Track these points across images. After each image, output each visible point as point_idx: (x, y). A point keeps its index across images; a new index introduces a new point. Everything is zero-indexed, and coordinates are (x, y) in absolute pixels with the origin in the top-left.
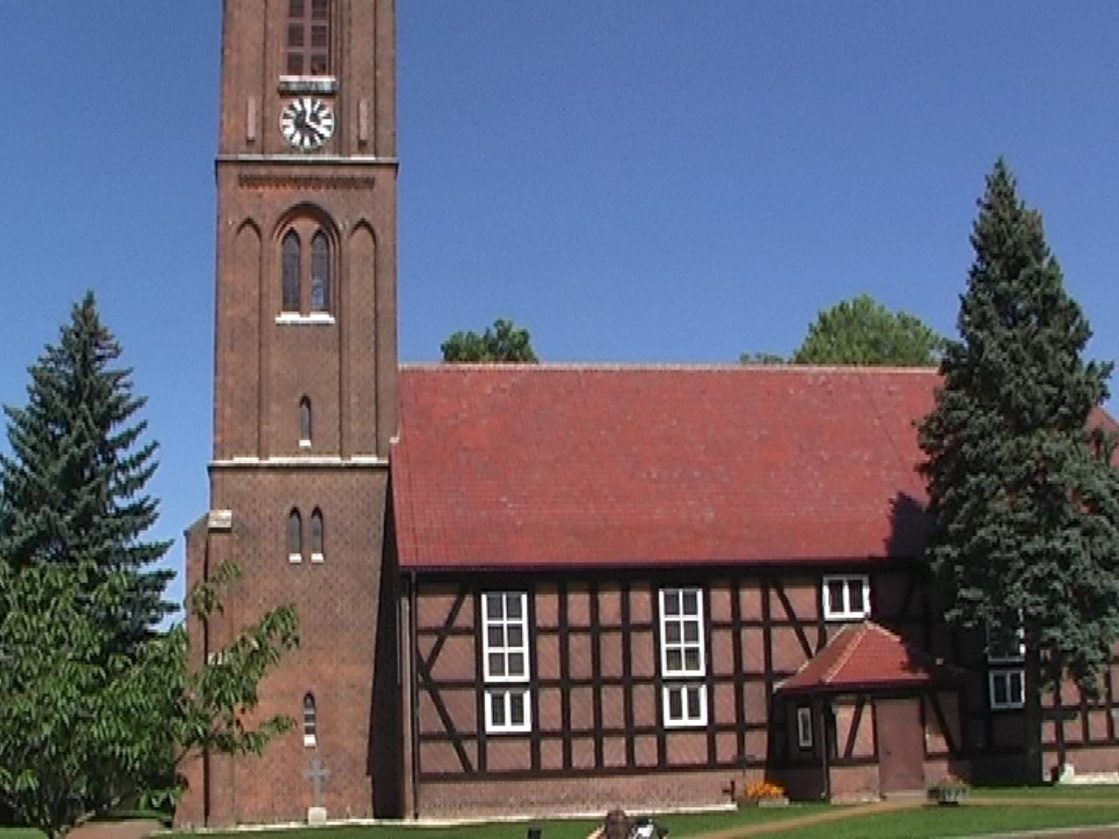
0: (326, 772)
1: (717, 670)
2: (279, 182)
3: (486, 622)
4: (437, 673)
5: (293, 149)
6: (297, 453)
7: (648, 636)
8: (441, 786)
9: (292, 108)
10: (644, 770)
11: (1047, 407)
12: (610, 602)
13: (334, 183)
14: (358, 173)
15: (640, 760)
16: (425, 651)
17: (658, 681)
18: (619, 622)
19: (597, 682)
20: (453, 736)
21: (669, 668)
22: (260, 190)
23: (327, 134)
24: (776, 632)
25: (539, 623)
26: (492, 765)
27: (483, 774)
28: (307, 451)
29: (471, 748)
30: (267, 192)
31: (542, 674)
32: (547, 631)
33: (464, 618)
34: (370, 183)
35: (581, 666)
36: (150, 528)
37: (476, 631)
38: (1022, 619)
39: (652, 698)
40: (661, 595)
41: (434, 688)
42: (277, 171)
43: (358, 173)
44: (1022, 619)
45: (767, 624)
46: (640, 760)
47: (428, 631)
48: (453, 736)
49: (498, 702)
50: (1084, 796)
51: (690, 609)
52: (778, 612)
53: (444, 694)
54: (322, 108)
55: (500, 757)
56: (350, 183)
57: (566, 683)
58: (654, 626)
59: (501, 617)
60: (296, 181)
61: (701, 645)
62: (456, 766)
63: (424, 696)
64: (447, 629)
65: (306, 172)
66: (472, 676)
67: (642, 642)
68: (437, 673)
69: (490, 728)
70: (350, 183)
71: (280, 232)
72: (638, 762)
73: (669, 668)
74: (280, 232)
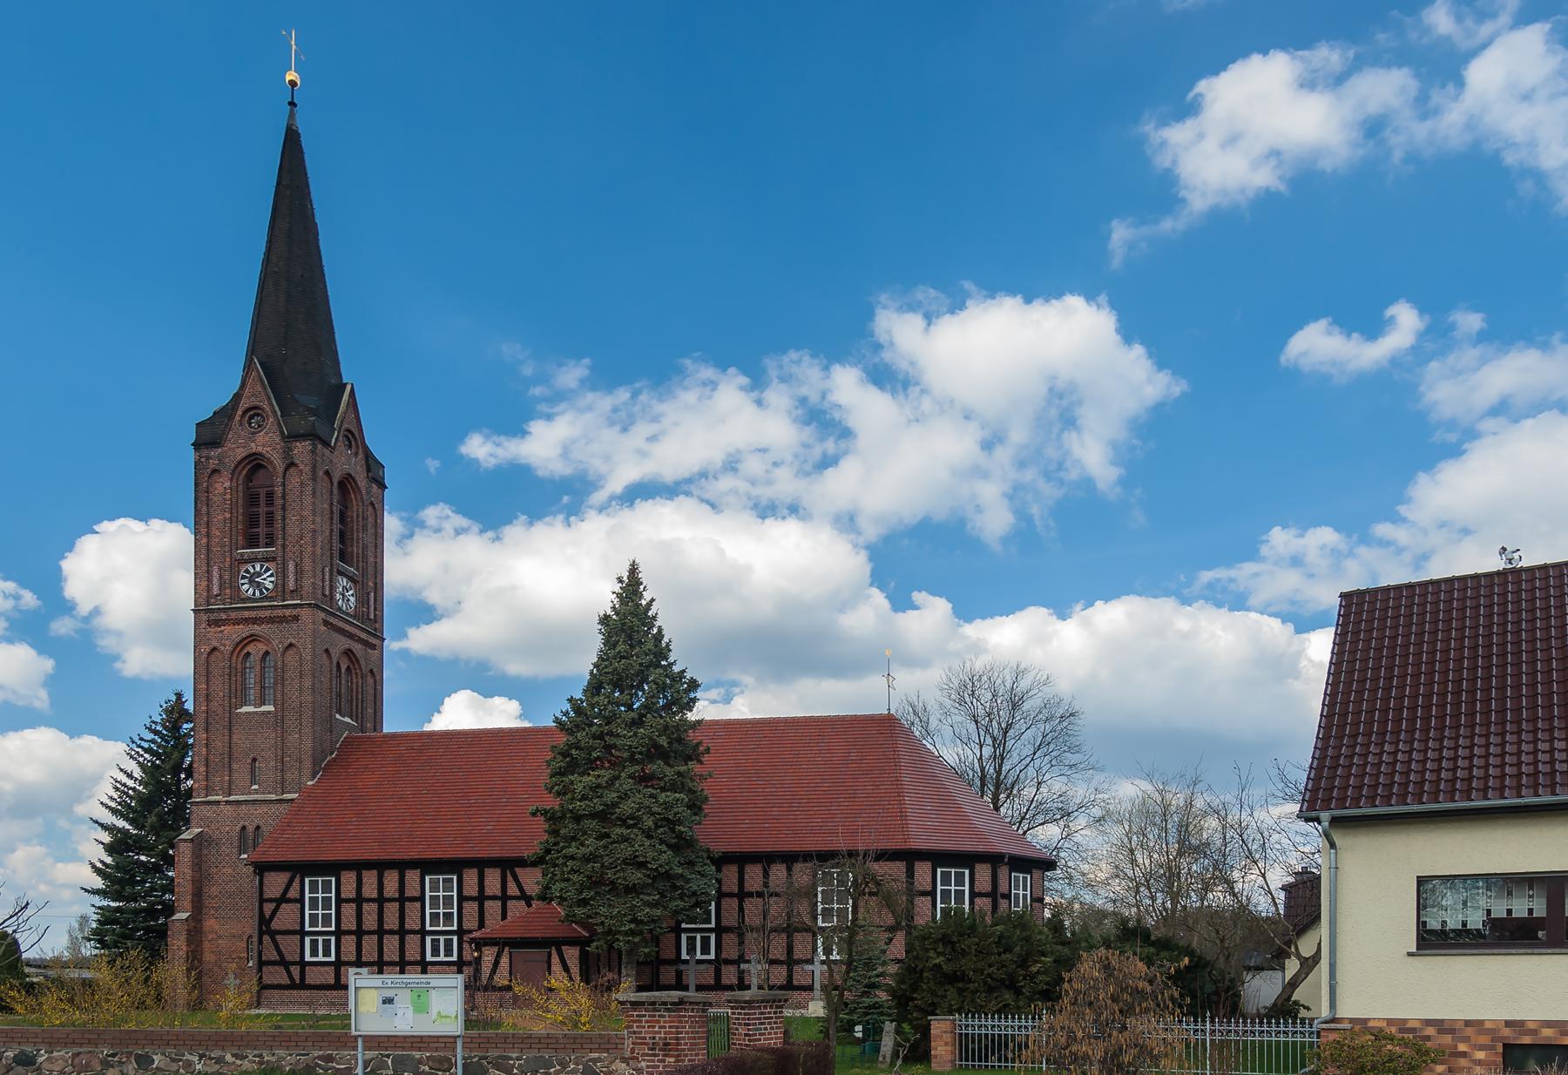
1: (344, 927)
2: (237, 622)
4: (275, 925)
5: (249, 599)
7: (418, 905)
8: (275, 992)
9: (247, 571)
10: (730, 988)
12: (391, 880)
13: (271, 620)
14: (288, 612)
15: (725, 981)
16: (267, 913)
17: (423, 933)
18: (397, 895)
19: (381, 932)
20: (283, 962)
21: (710, 923)
22: (223, 628)
23: (270, 586)
24: (510, 904)
25: (343, 896)
26: (308, 981)
27: (303, 986)
29: (295, 970)
30: (227, 629)
31: (725, 923)
32: (348, 901)
33: (293, 893)
34: (296, 618)
35: (370, 922)
37: (301, 901)
39: (419, 943)
40: (307, 880)
41: (273, 934)
42: (233, 615)
43: (288, 612)
45: (504, 898)
46: (725, 981)
47: (270, 900)
48: (283, 962)
52: (513, 889)
53: (278, 937)
54: (268, 570)
55: (313, 976)
58: (422, 899)
60: (246, 621)
62: (286, 981)
63: (266, 938)
64: (283, 899)
66: (298, 928)
67: (412, 909)
68: (275, 925)
69: (308, 958)
71: (240, 652)
72: (795, 983)
73: (710, 923)
74: (240, 652)
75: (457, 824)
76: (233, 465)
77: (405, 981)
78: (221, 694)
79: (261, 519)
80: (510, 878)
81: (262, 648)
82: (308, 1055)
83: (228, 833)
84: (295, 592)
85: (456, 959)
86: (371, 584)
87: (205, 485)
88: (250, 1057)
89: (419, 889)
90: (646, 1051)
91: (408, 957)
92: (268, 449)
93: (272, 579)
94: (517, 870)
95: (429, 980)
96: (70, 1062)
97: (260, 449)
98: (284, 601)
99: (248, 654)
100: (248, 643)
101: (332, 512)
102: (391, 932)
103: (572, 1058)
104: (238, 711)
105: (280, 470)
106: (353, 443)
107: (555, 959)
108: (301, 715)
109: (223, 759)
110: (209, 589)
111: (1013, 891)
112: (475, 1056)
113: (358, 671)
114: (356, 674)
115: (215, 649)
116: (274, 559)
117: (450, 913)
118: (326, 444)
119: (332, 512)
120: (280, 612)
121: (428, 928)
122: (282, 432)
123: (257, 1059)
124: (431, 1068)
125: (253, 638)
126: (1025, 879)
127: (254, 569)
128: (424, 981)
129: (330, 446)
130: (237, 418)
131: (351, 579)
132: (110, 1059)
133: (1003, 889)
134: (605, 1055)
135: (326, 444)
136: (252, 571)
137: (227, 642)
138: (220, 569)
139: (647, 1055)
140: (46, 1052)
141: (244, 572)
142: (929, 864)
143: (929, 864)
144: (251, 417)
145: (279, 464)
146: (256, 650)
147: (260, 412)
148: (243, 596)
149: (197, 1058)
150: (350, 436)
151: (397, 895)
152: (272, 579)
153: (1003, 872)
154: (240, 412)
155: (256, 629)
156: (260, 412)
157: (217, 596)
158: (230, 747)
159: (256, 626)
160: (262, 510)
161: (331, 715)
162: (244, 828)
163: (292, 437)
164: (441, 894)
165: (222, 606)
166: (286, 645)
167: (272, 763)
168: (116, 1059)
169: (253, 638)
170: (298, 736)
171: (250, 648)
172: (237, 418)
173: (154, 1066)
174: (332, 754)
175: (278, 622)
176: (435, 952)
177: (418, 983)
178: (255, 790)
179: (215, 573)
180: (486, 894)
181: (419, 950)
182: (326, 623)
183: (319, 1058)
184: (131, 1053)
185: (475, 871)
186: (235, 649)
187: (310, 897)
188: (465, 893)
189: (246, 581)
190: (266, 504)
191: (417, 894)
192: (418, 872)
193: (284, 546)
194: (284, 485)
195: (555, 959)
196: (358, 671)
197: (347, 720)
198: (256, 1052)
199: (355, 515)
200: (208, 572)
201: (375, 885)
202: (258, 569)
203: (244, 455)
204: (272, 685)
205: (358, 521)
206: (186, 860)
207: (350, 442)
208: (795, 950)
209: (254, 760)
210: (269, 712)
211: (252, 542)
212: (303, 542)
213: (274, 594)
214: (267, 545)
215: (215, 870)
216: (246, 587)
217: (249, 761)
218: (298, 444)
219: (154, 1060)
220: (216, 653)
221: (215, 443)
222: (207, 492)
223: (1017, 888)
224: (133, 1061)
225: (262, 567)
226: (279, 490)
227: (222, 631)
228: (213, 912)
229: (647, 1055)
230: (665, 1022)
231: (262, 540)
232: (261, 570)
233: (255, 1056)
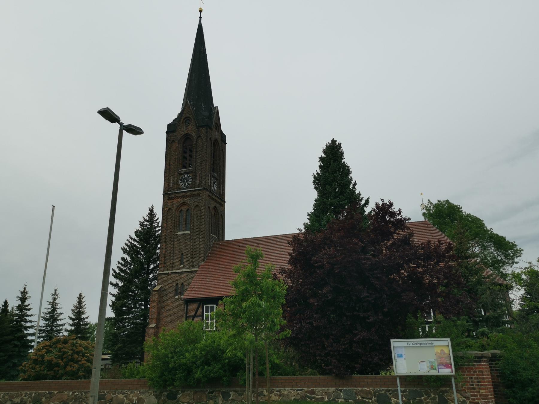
2: (178, 198)
6: (180, 269)
9: (182, 178)
11: (58, 353)
13: (190, 196)
14: (196, 193)
22: (173, 200)
28: (182, 268)
34: (199, 195)
38: (207, 321)
40: (205, 306)
42: (177, 195)
43: (196, 193)
44: (207, 321)
50: (483, 388)
54: (189, 176)
56: (195, 195)
59: (209, 320)
60: (182, 197)
65: (184, 194)
70: (195, 195)
75: (196, 287)
76: (179, 138)
77: (419, 342)
78: (171, 227)
81: (186, 207)
82: (302, 390)
83: (171, 287)
86: (222, 180)
87: (169, 146)
90: (469, 386)
93: (191, 180)
95: (432, 342)
96: (192, 397)
98: (168, 192)
99: (181, 210)
100: (181, 207)
101: (211, 153)
103: (432, 390)
104: (177, 234)
105: (195, 139)
106: (217, 128)
108: (200, 234)
109: (171, 254)
110: (169, 185)
112: (383, 390)
113: (218, 215)
114: (217, 217)
115: (170, 209)
116: (192, 172)
118: (210, 128)
119: (211, 153)
120: (193, 193)
122: (196, 125)
124: (362, 397)
125: (184, 204)
128: (430, 342)
129: (211, 129)
130: (182, 121)
131: (216, 179)
132: (210, 394)
134: (448, 388)
135: (210, 128)
137: (174, 206)
138: (173, 177)
139: (470, 388)
140: (181, 392)
144: (186, 121)
145: (195, 136)
146: (184, 208)
147: (189, 118)
150: (217, 126)
152: (191, 180)
154: (182, 119)
155: (185, 200)
156: (189, 118)
157: (171, 188)
158: (173, 249)
159: (185, 199)
161: (209, 233)
162: (177, 284)
163: (199, 127)
165: (173, 192)
166: (195, 205)
167: (189, 255)
168: (213, 395)
169: (184, 204)
170: (198, 243)
171: (182, 208)
172: (182, 121)
173: (231, 398)
174: (209, 250)
175: (192, 197)
177: (426, 344)
178: (182, 267)
179: (171, 179)
182: (209, 196)
183: (307, 392)
184: (219, 391)
186: (177, 208)
189: (182, 181)
193: (196, 167)
194: (196, 144)
196: (218, 215)
197: (214, 235)
198: (278, 389)
199: (217, 154)
200: (169, 179)
203: (183, 134)
204: (189, 222)
205: (218, 157)
207: (216, 128)
209: (182, 254)
210: (188, 234)
211: (184, 166)
212: (202, 165)
213: (191, 186)
214: (190, 167)
215: (165, 304)
217: (180, 255)
218: (202, 129)
219: (230, 395)
220: (170, 211)
221: (173, 131)
222: (170, 149)
224: (221, 395)
226: (194, 146)
227: (172, 202)
229: (470, 388)
230: (476, 368)
231: (187, 165)
232: (187, 177)
233: (277, 391)
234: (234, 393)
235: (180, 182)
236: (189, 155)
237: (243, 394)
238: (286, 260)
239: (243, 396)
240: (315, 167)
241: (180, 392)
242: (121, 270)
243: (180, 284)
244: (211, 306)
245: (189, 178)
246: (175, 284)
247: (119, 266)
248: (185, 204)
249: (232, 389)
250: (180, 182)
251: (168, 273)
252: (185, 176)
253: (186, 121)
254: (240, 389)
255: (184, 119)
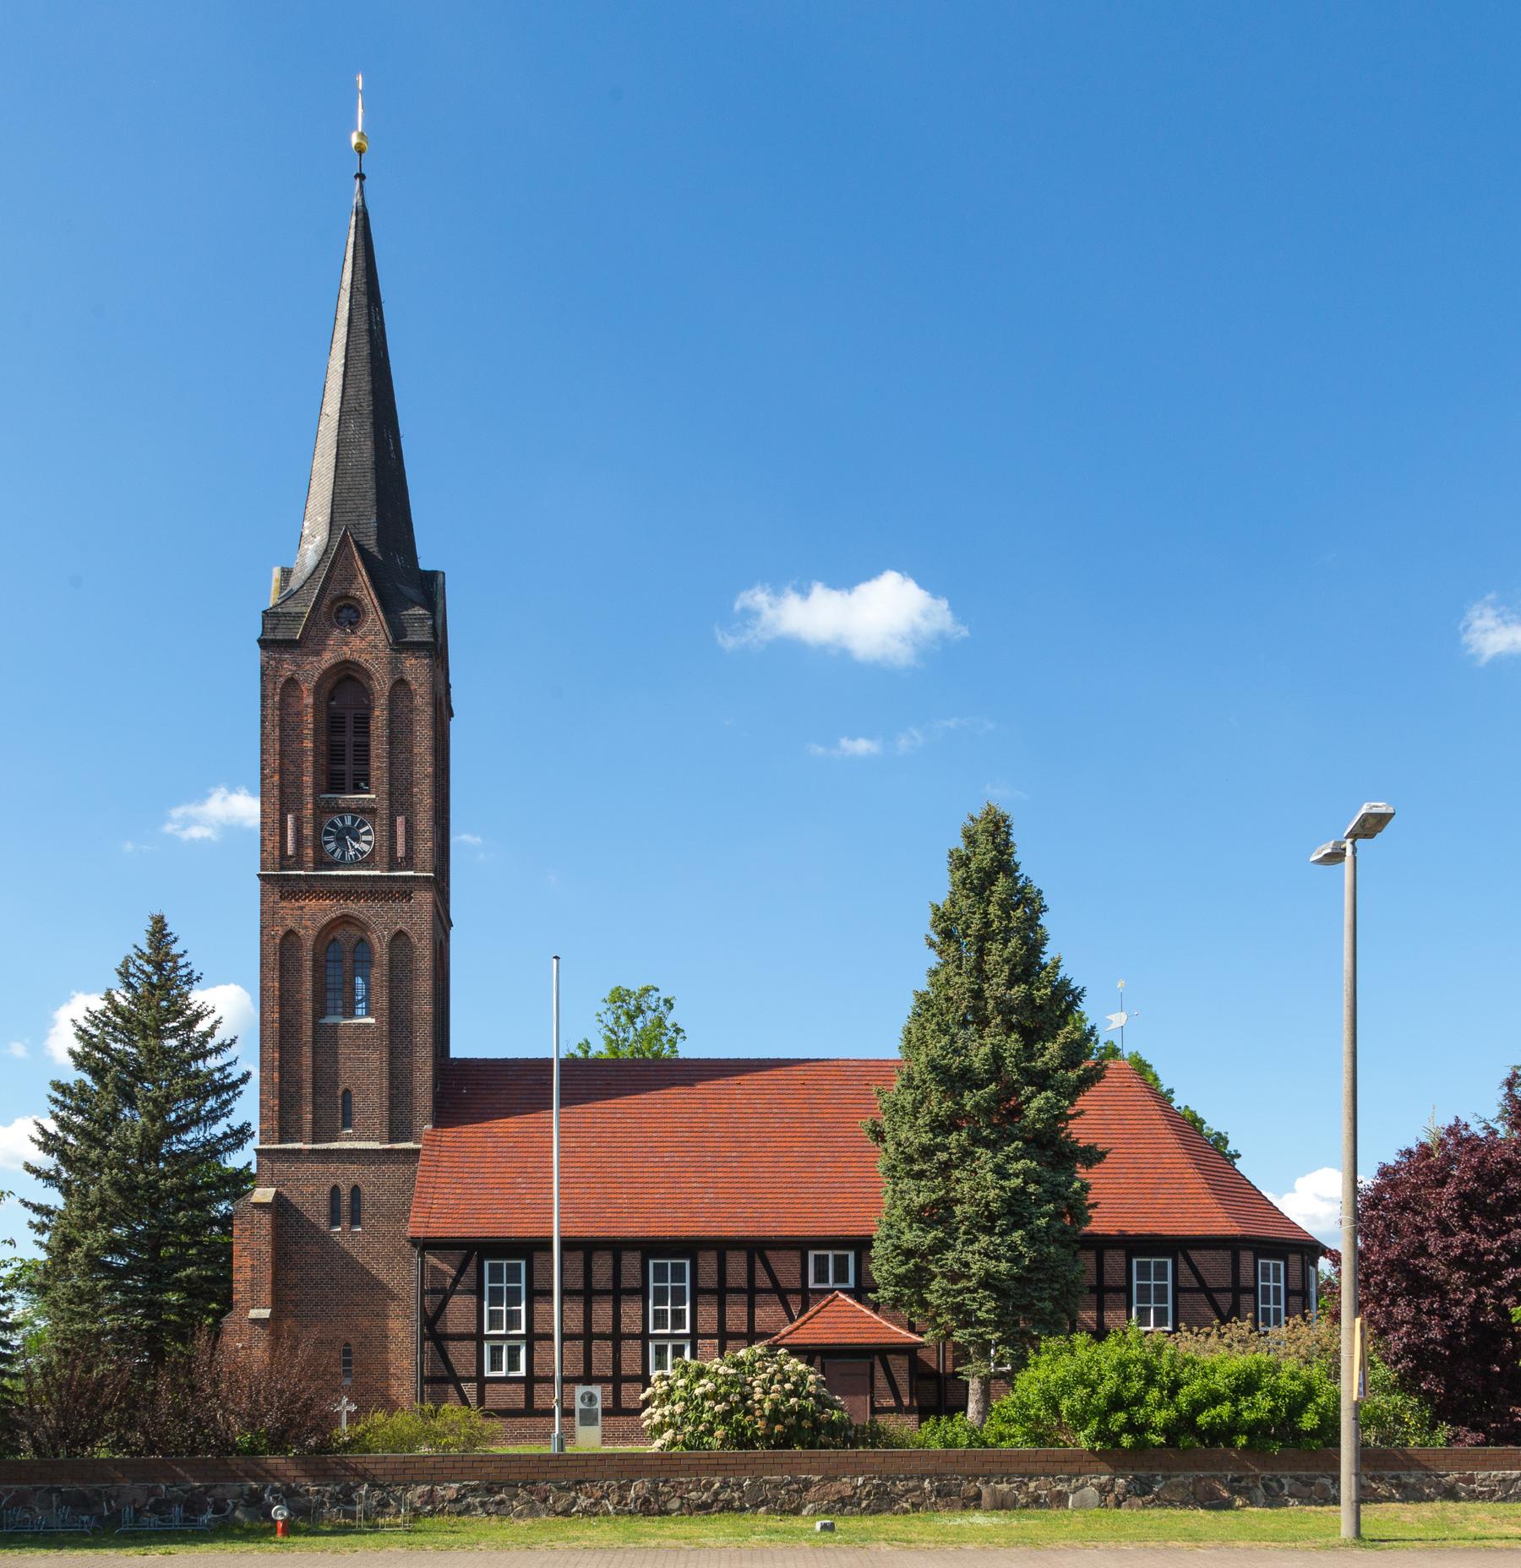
0: (353, 1408)
3: (652, 1285)
9: (333, 825)
17: (645, 1337)
18: (610, 1286)
22: (302, 903)
28: (350, 1138)
30: (311, 904)
36: (1214, 1123)
49: (496, 1351)
51: (1161, 1274)
52: (763, 1280)
57: (617, 1337)
59: (667, 1310)
61: (1169, 1305)
69: (488, 1373)
73: (684, 1328)
79: (347, 751)
80: (759, 1265)
83: (313, 1194)
84: (409, 862)
85: (486, 1375)
88: (1387, 1479)
89: (639, 1277)
91: (626, 1370)
92: (368, 657)
94: (768, 1253)
96: (1191, 1489)
97: (356, 656)
99: (334, 940)
102: (602, 1336)
107: (879, 1373)
111: (1260, 1283)
117: (663, 1310)
121: (486, 1332)
123: (1394, 1481)
126: (1277, 1268)
127: (343, 821)
132: (1235, 1484)
133: (1246, 1279)
136: (340, 825)
141: (330, 825)
142: (1122, 1253)
143: (1122, 1253)
144: (340, 610)
148: (327, 860)
149: (1331, 1481)
151: (610, 1286)
153: (1246, 1258)
155: (353, 907)
160: (349, 738)
162: (335, 1190)
164: (505, 1285)
168: (1243, 1484)
176: (496, 1365)
180: (728, 1285)
181: (639, 1361)
185: (714, 1254)
187: (490, 1288)
188: (701, 1284)
189: (331, 838)
190: (355, 732)
191: (636, 1284)
192: (638, 1254)
195: (879, 1373)
201: (580, 1272)
202: (348, 822)
206: (263, 1233)
208: (623, 1365)
215: (295, 1248)
216: (332, 846)
223: (1266, 1277)
224: (1260, 1486)
225: (354, 820)
227: (302, 908)
228: (291, 1307)
231: (349, 782)
232: (353, 823)
234: (1292, 1481)
235: (326, 839)
236: (355, 746)
237: (1313, 1484)
238: (1108, 1166)
239: (1313, 1488)
240: (940, 887)
241: (1159, 1478)
242: (64, 1125)
243: (345, 1191)
244: (672, 1264)
245: (362, 831)
246: (327, 1189)
247: (57, 1110)
248: (352, 920)
249: (1286, 1473)
250: (326, 839)
251: (300, 1150)
252: (342, 820)
253: (340, 610)
254: (1305, 1473)
255: (333, 602)
